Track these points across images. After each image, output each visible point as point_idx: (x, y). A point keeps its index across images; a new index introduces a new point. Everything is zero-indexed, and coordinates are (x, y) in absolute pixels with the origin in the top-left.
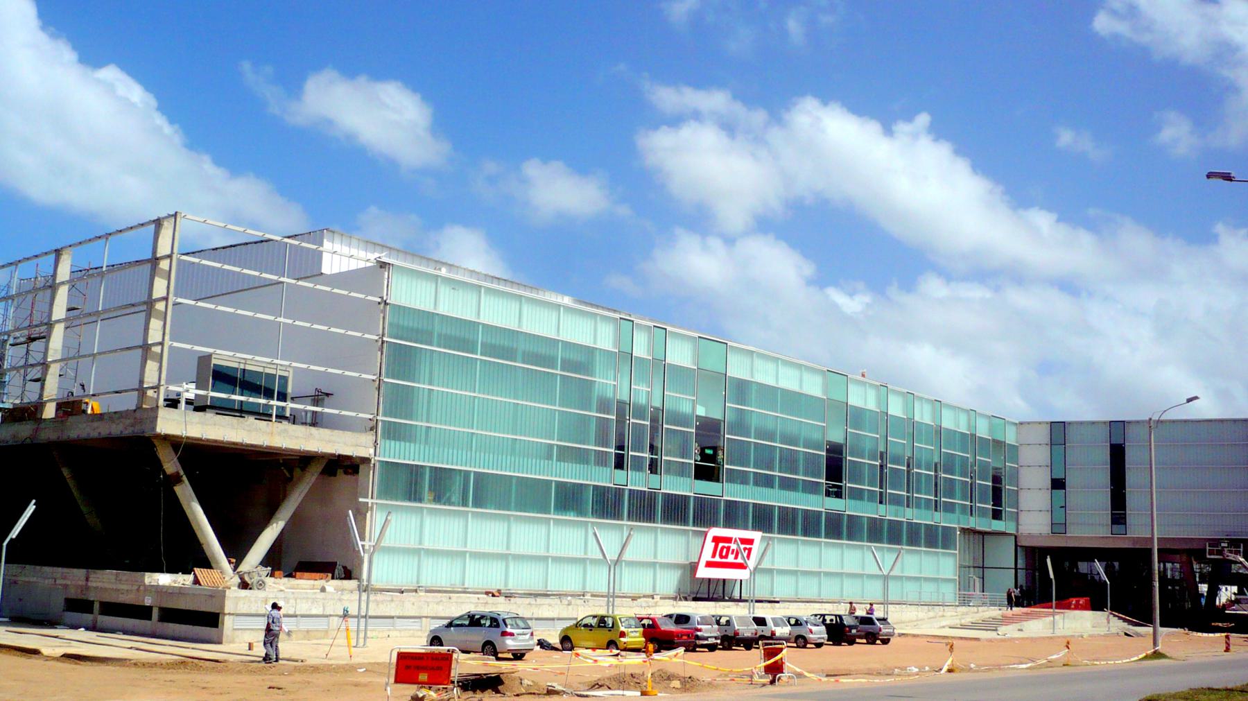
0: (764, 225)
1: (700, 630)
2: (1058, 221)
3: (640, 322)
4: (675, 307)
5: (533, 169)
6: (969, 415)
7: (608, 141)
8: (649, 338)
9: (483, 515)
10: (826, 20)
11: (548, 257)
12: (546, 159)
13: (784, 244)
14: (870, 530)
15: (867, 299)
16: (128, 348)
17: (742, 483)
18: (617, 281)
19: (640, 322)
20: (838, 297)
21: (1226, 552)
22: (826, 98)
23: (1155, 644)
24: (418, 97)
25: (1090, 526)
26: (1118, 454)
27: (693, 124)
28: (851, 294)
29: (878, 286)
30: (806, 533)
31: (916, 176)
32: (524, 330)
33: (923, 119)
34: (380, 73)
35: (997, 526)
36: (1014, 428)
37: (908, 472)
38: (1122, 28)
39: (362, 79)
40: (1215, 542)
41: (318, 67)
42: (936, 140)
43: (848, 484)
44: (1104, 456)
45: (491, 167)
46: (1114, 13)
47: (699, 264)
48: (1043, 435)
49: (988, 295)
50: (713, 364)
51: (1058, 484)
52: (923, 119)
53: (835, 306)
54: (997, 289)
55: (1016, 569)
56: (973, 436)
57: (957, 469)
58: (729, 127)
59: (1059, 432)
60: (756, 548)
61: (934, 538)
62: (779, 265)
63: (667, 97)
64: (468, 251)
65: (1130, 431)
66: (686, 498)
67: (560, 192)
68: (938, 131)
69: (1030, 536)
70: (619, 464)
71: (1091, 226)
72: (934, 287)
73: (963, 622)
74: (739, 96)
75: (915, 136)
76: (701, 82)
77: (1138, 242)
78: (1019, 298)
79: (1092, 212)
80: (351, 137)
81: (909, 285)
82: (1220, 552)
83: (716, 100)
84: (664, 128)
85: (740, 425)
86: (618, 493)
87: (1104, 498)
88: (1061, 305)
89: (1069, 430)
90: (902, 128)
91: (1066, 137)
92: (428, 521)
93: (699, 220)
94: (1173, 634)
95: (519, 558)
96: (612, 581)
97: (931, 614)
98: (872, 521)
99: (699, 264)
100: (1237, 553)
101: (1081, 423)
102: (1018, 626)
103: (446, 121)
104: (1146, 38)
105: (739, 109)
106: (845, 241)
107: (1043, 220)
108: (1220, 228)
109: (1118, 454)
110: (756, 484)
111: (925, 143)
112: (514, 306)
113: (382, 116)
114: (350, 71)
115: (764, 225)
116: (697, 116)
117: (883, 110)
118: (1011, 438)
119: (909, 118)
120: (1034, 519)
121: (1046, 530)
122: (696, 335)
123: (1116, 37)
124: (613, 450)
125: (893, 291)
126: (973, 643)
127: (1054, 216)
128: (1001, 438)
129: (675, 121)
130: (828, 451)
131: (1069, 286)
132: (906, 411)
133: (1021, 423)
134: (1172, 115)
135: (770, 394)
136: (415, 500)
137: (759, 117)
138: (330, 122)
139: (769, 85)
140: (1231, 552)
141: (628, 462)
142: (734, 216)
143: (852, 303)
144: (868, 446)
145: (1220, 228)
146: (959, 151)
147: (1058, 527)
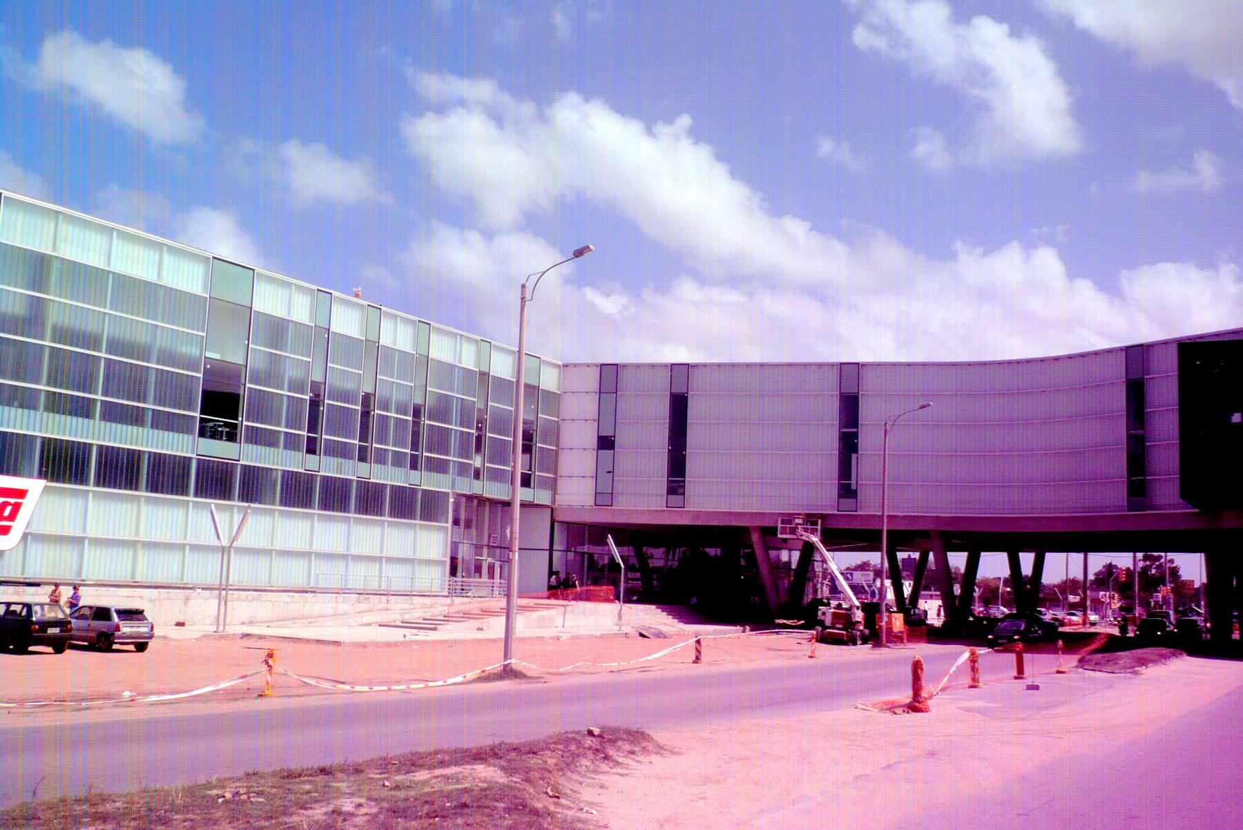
0: (533, 222)
1: (1062, 624)
2: (811, 229)
3: (436, 325)
4: (441, 304)
5: (293, 150)
6: (312, 296)
7: (372, 125)
8: (207, 272)
9: (428, 527)
10: (593, 16)
11: (306, 241)
12: (306, 141)
13: (542, 241)
14: (359, 497)
15: (624, 300)
16: (849, 444)
17: (294, 449)
18: (373, 272)
19: (436, 325)
20: (591, 294)
21: (800, 530)
22: (588, 95)
23: (506, 656)
24: (169, 68)
25: (643, 501)
26: (679, 405)
27: (460, 110)
28: (607, 295)
29: (634, 289)
30: (325, 505)
31: (675, 177)
32: (112, 269)
33: (685, 121)
34: (125, 39)
35: (543, 497)
36: (555, 372)
37: (416, 424)
38: (880, 43)
39: (107, 45)
40: (788, 519)
41: (58, 27)
42: (696, 143)
43: (244, 422)
44: (663, 408)
45: (249, 146)
46: (874, 28)
47: (460, 257)
48: (591, 381)
49: (743, 299)
50: (232, 293)
51: (606, 443)
52: (685, 121)
53: (593, 305)
54: (751, 295)
55: (551, 550)
56: (484, 375)
57: (454, 416)
58: (497, 117)
59: (611, 377)
60: (28, 504)
61: (404, 505)
62: (533, 257)
63: (432, 85)
64: (220, 236)
65: (697, 381)
66: (188, 460)
67: (322, 176)
68: (697, 135)
69: (570, 508)
70: (311, 450)
71: (839, 234)
72: (688, 289)
73: (407, 617)
74: (504, 86)
75: (677, 138)
76: (466, 71)
77: (890, 254)
78: (773, 305)
79: (844, 222)
80: (96, 107)
81: (663, 288)
82: (793, 531)
83: (483, 90)
84: (430, 115)
85: (271, 375)
86: (310, 478)
87: (660, 463)
88: (812, 313)
89: (625, 376)
90: (662, 129)
91: (826, 147)
92: (144, 508)
93: (461, 211)
94: (725, 632)
95: (358, 558)
96: (226, 568)
97: (363, 606)
98: (396, 490)
99: (460, 257)
100: (814, 532)
101: (638, 366)
102: (477, 623)
103: (200, 94)
104: (903, 54)
105: (506, 98)
106: (598, 238)
107: (796, 227)
108: (958, 245)
109: (679, 405)
110: (155, 425)
111: (685, 145)
112: (153, 255)
113: (132, 86)
114: (92, 32)
115: (533, 222)
116: (462, 103)
117: (644, 108)
118: (549, 381)
119: (670, 119)
120: (576, 494)
121: (590, 501)
122: (417, 319)
123: (876, 52)
124: (305, 433)
125: (648, 295)
126: (331, 648)
127: (808, 225)
128: (534, 382)
129: (441, 109)
130: (206, 372)
131: (819, 293)
132: (416, 344)
133: (566, 366)
134: (926, 131)
135: (86, 278)
136: (81, 483)
137: (528, 109)
138: (73, 90)
139: (534, 77)
140: (806, 530)
141: (422, 463)
142: (502, 209)
143: (610, 304)
144: (395, 397)
145: (958, 245)
146: (719, 157)
147: (604, 498)
